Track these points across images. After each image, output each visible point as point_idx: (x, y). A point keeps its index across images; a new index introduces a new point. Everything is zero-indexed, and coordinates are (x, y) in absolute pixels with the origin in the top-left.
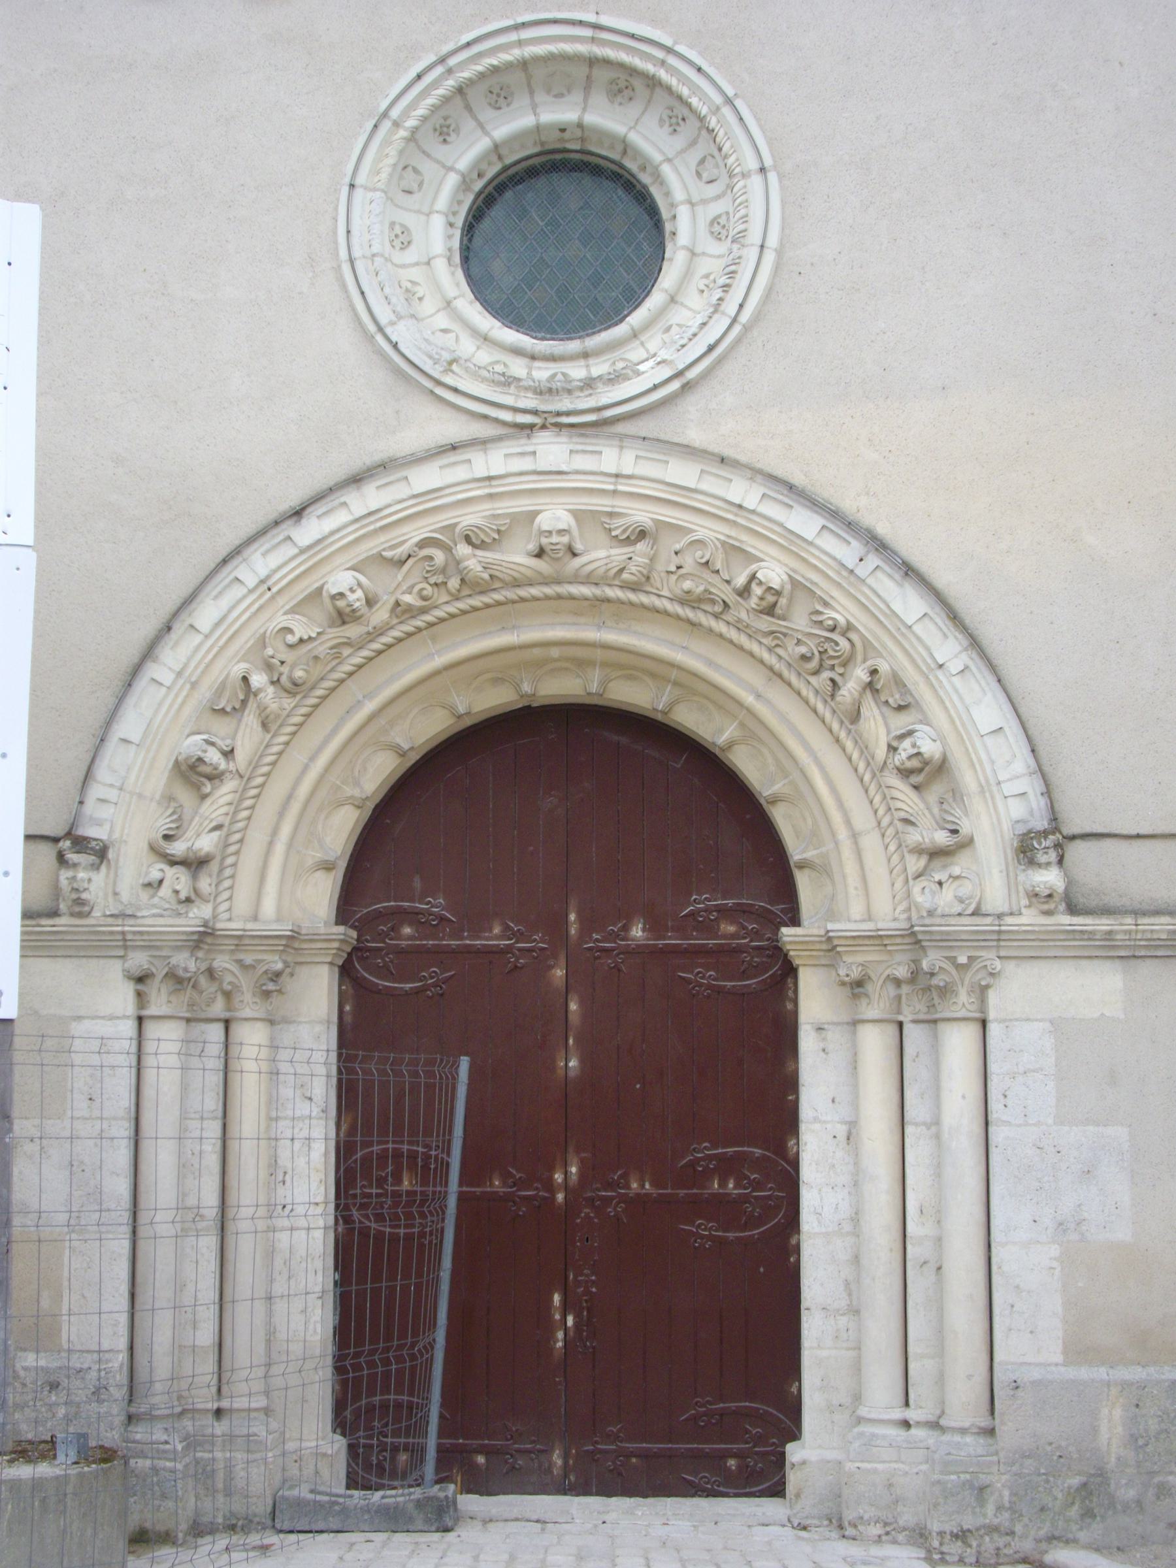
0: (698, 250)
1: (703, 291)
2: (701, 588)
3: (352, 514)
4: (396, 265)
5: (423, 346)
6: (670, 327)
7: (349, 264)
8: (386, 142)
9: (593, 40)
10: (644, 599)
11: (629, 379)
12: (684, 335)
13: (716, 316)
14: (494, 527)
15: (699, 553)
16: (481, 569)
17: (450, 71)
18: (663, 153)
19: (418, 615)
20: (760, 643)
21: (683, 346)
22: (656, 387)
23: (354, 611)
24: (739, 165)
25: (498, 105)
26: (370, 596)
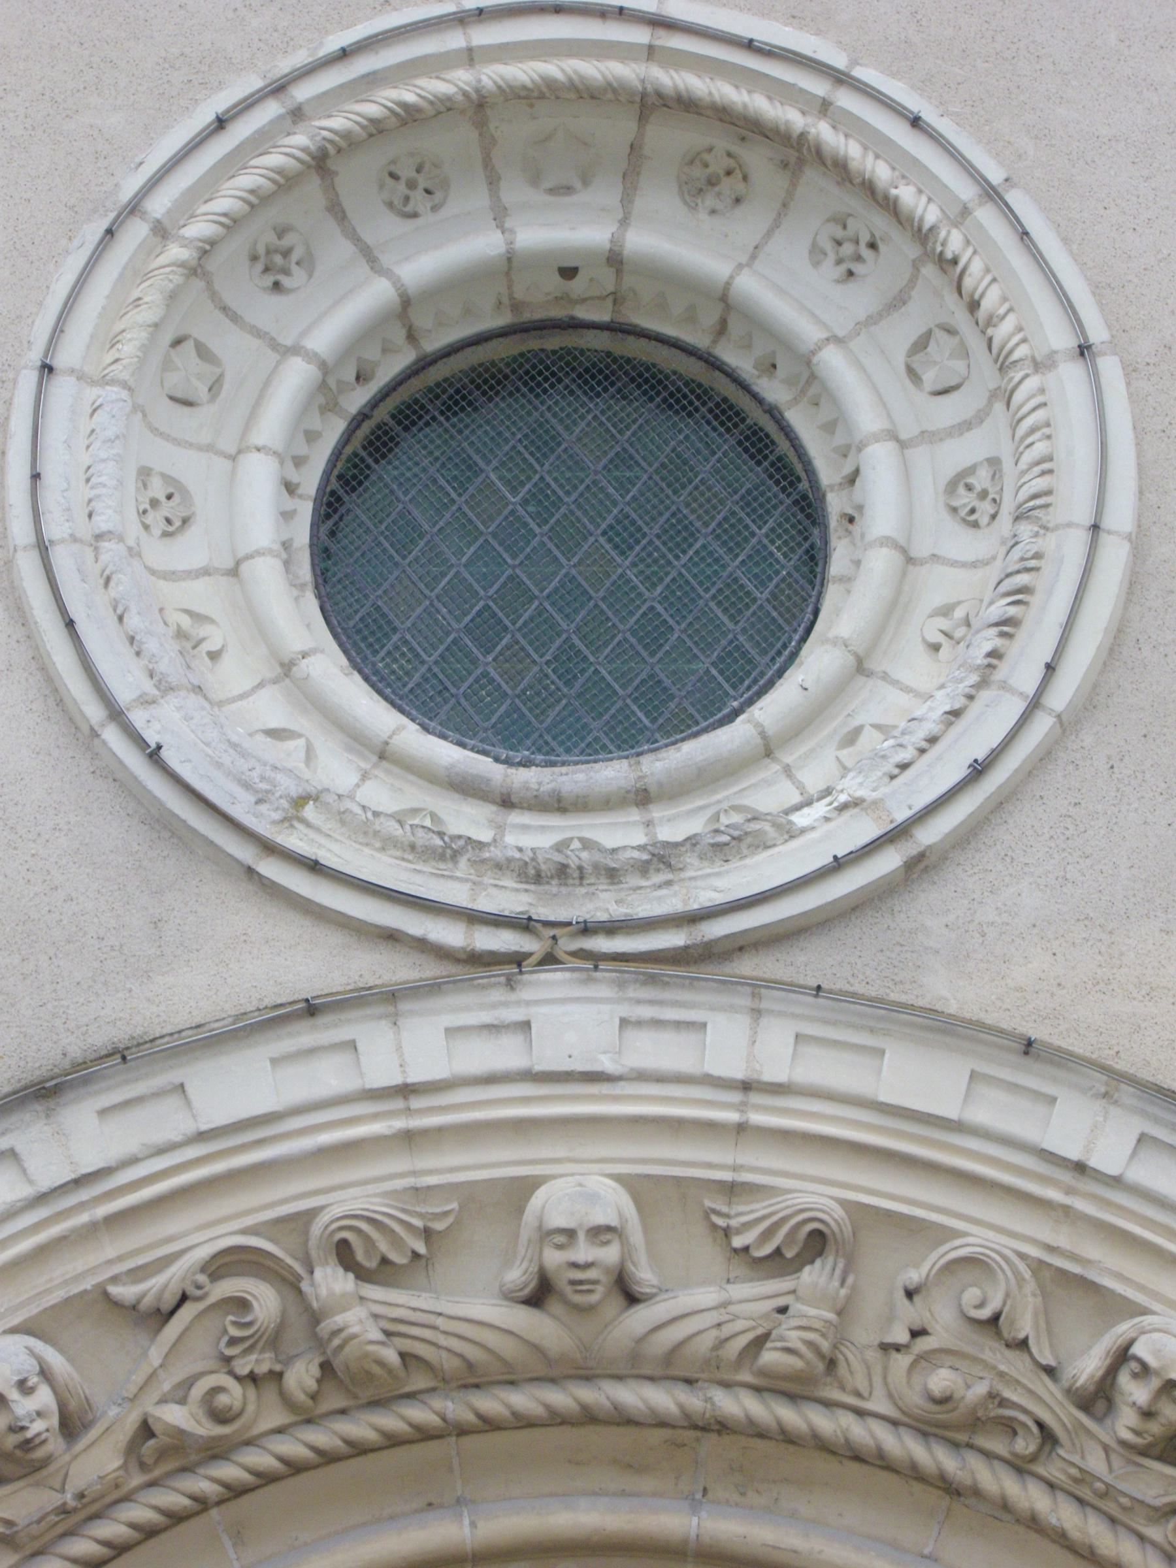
0: (921, 550)
1: (936, 648)
2: (980, 1389)
3: (31, 1182)
4: (153, 572)
5: (226, 760)
6: (858, 730)
7: (34, 555)
8: (135, 273)
9: (651, 52)
10: (823, 1422)
11: (767, 847)
12: (905, 740)
13: (985, 695)
14: (417, 1222)
15: (972, 1295)
16: (380, 1336)
17: (297, 114)
18: (824, 325)
19: (200, 1463)
20: (1142, 1538)
21: (904, 767)
22: (838, 865)
23: (27, 1445)
24: (1024, 340)
25: (409, 209)
26: (73, 1405)
